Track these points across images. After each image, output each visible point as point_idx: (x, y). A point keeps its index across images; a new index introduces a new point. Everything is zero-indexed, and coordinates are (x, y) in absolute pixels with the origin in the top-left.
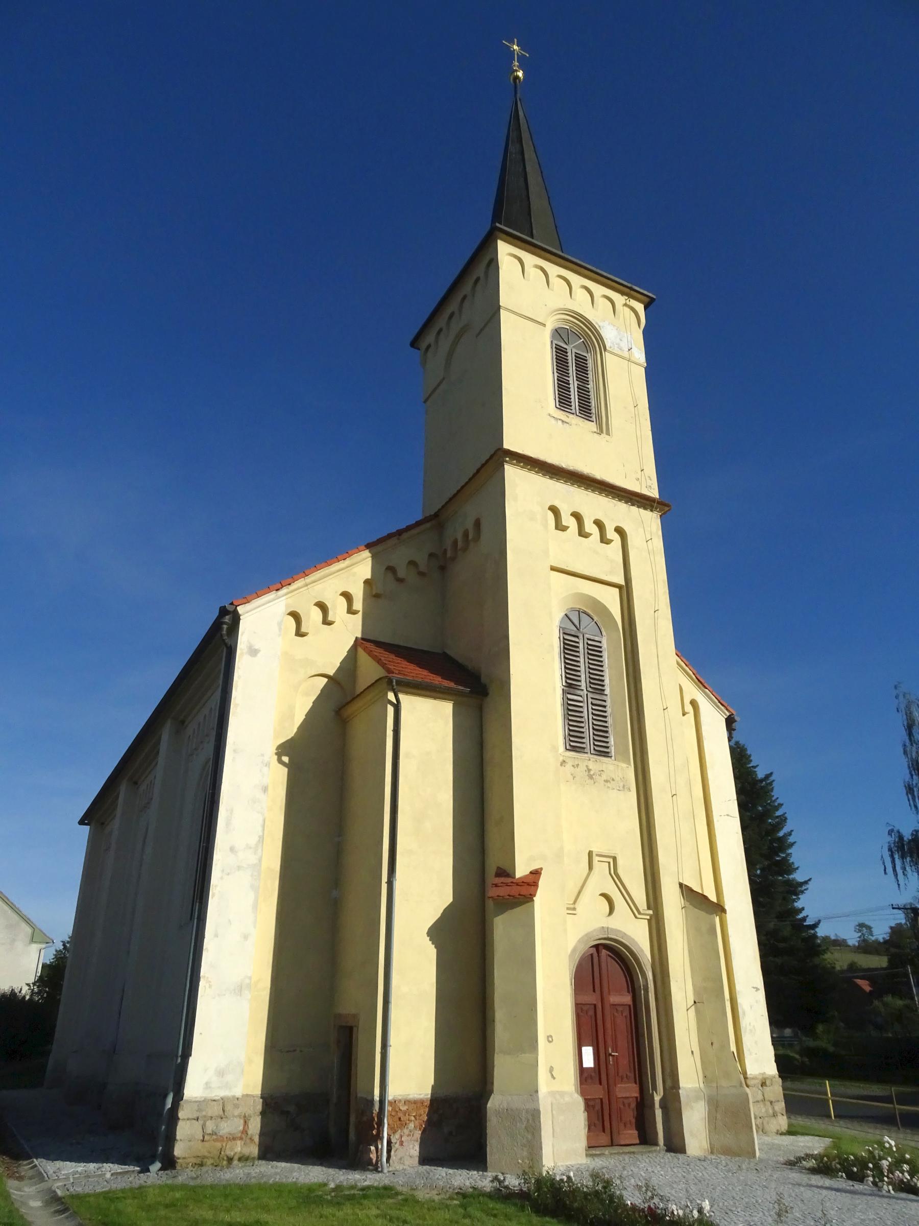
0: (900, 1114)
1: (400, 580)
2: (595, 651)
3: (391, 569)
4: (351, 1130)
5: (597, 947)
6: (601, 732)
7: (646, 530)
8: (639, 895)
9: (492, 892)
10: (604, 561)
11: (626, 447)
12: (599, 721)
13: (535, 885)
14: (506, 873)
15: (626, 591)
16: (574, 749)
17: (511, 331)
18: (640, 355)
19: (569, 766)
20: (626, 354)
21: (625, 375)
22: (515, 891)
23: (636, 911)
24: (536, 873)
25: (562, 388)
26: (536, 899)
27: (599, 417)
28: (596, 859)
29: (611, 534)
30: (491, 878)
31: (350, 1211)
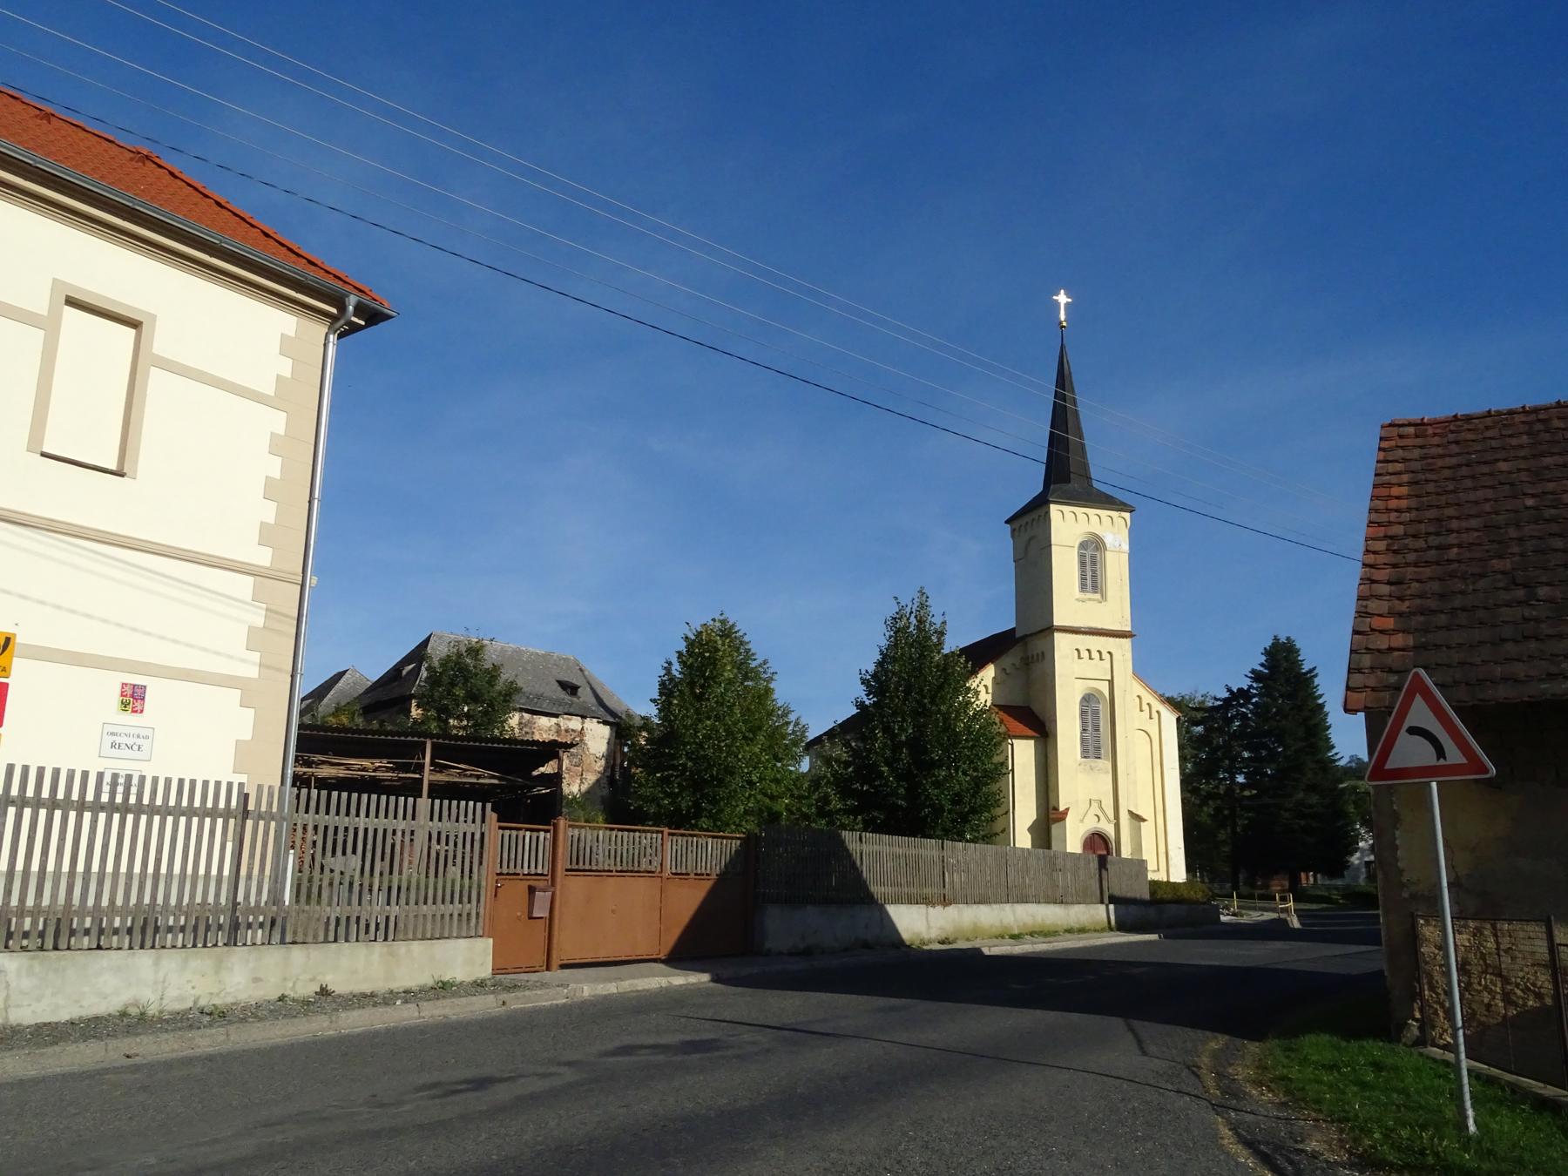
2: (1096, 713)
4: (1032, 909)
6: (1098, 748)
7: (1122, 650)
8: (1111, 815)
10: (1100, 669)
11: (1115, 609)
12: (1100, 739)
14: (1056, 809)
15: (1111, 682)
18: (1126, 547)
21: (1117, 567)
23: (1109, 821)
25: (1083, 578)
29: (1106, 656)
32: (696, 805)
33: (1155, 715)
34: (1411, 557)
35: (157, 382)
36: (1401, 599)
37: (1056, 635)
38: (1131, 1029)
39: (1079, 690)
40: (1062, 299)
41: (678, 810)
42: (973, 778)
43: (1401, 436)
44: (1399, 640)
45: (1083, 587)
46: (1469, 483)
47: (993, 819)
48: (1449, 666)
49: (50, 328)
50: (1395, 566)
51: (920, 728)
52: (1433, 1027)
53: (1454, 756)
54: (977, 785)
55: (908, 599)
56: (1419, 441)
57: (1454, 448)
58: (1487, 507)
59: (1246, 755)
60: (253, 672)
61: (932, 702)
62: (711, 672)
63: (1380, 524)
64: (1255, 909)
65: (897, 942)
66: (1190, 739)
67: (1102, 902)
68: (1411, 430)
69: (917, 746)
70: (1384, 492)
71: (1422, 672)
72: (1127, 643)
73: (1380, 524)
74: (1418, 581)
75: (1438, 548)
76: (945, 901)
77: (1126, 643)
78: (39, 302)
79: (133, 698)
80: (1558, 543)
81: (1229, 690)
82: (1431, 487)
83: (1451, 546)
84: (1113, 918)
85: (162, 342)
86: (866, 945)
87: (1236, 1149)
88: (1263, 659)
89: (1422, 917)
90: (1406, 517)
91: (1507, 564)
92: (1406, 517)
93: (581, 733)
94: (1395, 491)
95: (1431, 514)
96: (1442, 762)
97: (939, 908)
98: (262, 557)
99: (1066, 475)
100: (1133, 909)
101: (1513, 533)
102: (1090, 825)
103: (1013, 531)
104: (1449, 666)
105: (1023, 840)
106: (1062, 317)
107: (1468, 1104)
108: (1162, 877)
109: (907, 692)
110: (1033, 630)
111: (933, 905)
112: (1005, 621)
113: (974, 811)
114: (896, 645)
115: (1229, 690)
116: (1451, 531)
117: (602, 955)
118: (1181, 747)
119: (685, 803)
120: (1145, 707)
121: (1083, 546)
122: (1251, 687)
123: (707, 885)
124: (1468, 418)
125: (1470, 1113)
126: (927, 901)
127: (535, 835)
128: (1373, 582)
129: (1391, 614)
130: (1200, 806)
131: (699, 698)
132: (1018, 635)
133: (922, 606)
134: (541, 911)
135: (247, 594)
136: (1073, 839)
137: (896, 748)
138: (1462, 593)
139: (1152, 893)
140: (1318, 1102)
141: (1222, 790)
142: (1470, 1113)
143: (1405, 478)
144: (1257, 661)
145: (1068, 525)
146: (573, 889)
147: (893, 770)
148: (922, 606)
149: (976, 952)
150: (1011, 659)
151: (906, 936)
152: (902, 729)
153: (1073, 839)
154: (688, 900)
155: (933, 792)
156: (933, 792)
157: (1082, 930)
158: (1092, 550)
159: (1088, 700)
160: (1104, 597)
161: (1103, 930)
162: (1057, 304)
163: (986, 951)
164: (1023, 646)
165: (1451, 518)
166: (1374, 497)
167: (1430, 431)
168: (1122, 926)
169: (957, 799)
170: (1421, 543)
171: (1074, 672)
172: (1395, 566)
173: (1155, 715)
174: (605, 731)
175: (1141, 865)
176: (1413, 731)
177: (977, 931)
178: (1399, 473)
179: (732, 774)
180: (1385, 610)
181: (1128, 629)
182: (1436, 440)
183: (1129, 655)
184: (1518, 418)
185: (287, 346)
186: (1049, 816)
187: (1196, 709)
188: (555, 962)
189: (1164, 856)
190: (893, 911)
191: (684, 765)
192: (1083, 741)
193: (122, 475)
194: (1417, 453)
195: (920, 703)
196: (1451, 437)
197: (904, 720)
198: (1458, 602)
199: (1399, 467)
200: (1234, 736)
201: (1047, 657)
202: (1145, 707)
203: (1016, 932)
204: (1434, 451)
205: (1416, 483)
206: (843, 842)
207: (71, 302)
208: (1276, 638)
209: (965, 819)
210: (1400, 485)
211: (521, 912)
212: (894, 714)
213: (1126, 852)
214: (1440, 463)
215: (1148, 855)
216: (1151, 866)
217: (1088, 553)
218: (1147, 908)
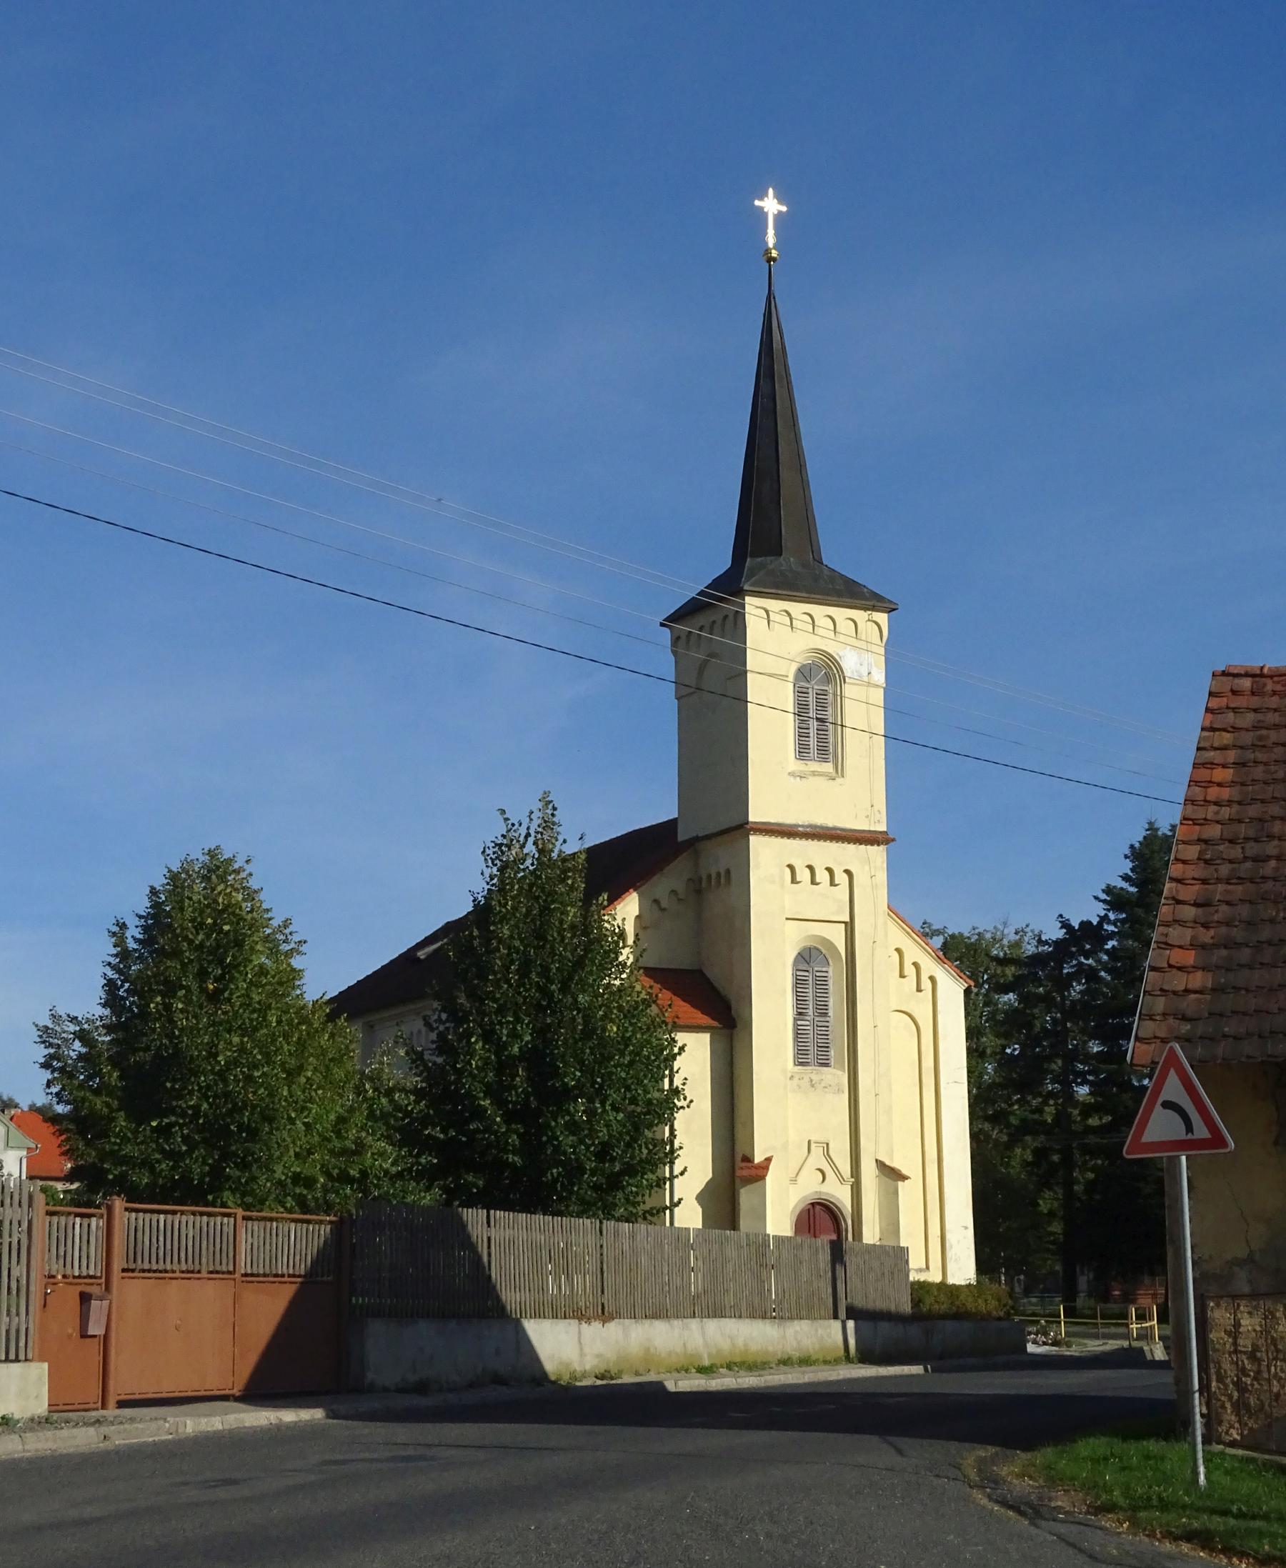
1: (663, 910)
2: (821, 982)
3: (656, 901)
5: (813, 1204)
7: (871, 865)
8: (846, 1169)
9: (739, 1173)
11: (858, 789)
12: (827, 1036)
13: (767, 1168)
14: (748, 1159)
15: (850, 927)
16: (801, 1064)
17: (756, 688)
18: (879, 677)
19: (796, 1080)
20: (866, 679)
22: (753, 1172)
23: (842, 1180)
24: (769, 1160)
25: (802, 734)
26: (768, 1178)
27: (836, 756)
28: (813, 1146)
29: (841, 878)
30: (739, 1163)
31: (798, 1328)
33: (927, 984)
34: (1225, 870)
36: (1206, 926)
37: (754, 840)
38: (890, 1444)
39: (791, 941)
40: (771, 205)
41: (186, 1178)
42: (630, 1115)
43: (1234, 692)
45: (802, 751)
47: (660, 1183)
48: (1244, 1014)
50: (1204, 882)
51: (542, 1033)
52: (1220, 1423)
53: (1201, 1132)
54: (637, 1128)
55: (524, 809)
56: (1255, 702)
59: (1095, 1048)
61: (564, 989)
63: (1195, 822)
64: (1096, 1337)
66: (992, 1017)
67: (836, 1317)
68: (1246, 683)
69: (539, 1061)
71: (1177, 1047)
73: (1195, 822)
74: (1228, 903)
75: (1255, 859)
76: (604, 1315)
77: (877, 854)
81: (1065, 925)
82: (1259, 772)
83: (1269, 858)
84: (852, 1342)
86: (498, 1380)
87: (990, 1505)
88: (1127, 867)
89: (1211, 1298)
90: (1226, 812)
92: (1226, 812)
95: (1253, 811)
96: (1190, 1136)
97: (596, 1325)
99: (772, 540)
100: (884, 1326)
102: (809, 1187)
103: (676, 641)
104: (1244, 1014)
105: (689, 1216)
106: (771, 240)
107: (1200, 1461)
108: (935, 1277)
110: (713, 828)
111: (589, 1320)
112: (655, 804)
113: (630, 1170)
114: (502, 890)
115: (1065, 925)
116: (1271, 837)
117: (167, 1388)
118: (972, 1033)
120: (910, 970)
121: (804, 673)
122: (1104, 919)
125: (1202, 1469)
126: (580, 1315)
127: (86, 1221)
128: (1178, 902)
129: (1193, 945)
130: (1009, 1146)
132: (682, 836)
133: (548, 824)
134: (95, 1329)
136: (778, 1211)
137: (504, 1066)
138: (1272, 921)
139: (916, 1303)
140: (1073, 1479)
142: (1202, 1469)
145: (778, 635)
147: (499, 1102)
150: (668, 882)
151: (550, 1366)
152: (514, 1035)
153: (778, 1211)
154: (267, 1310)
155: (567, 1140)
156: (567, 1140)
157: (805, 1361)
158: (818, 682)
159: (809, 958)
160: (839, 770)
161: (836, 1361)
162: (762, 214)
163: (671, 1386)
165: (1274, 818)
166: (1193, 782)
167: (1270, 686)
168: (866, 1355)
170: (1236, 852)
171: (782, 908)
172: (1204, 882)
173: (927, 984)
175: (900, 1255)
176: (1168, 1105)
177: (649, 1358)
178: (1224, 748)
179: (270, 1120)
180: (1187, 940)
181: (882, 827)
183: (882, 877)
186: (737, 1171)
187: (1003, 962)
188: (112, 1401)
189: (939, 1240)
191: (196, 1108)
192: (798, 1033)
194: (1250, 718)
195: (544, 991)
197: (518, 1020)
198: (1265, 934)
199: (1227, 738)
200: (1074, 1011)
201: (736, 878)
202: (910, 970)
203: (706, 1363)
205: (1244, 765)
206: (463, 1226)
208: (1152, 827)
209: (614, 1183)
210: (1224, 766)
211: (73, 1329)
212: (501, 1011)
213: (871, 1234)
215: (910, 1238)
216: (916, 1261)
217: (814, 686)
218: (913, 1324)
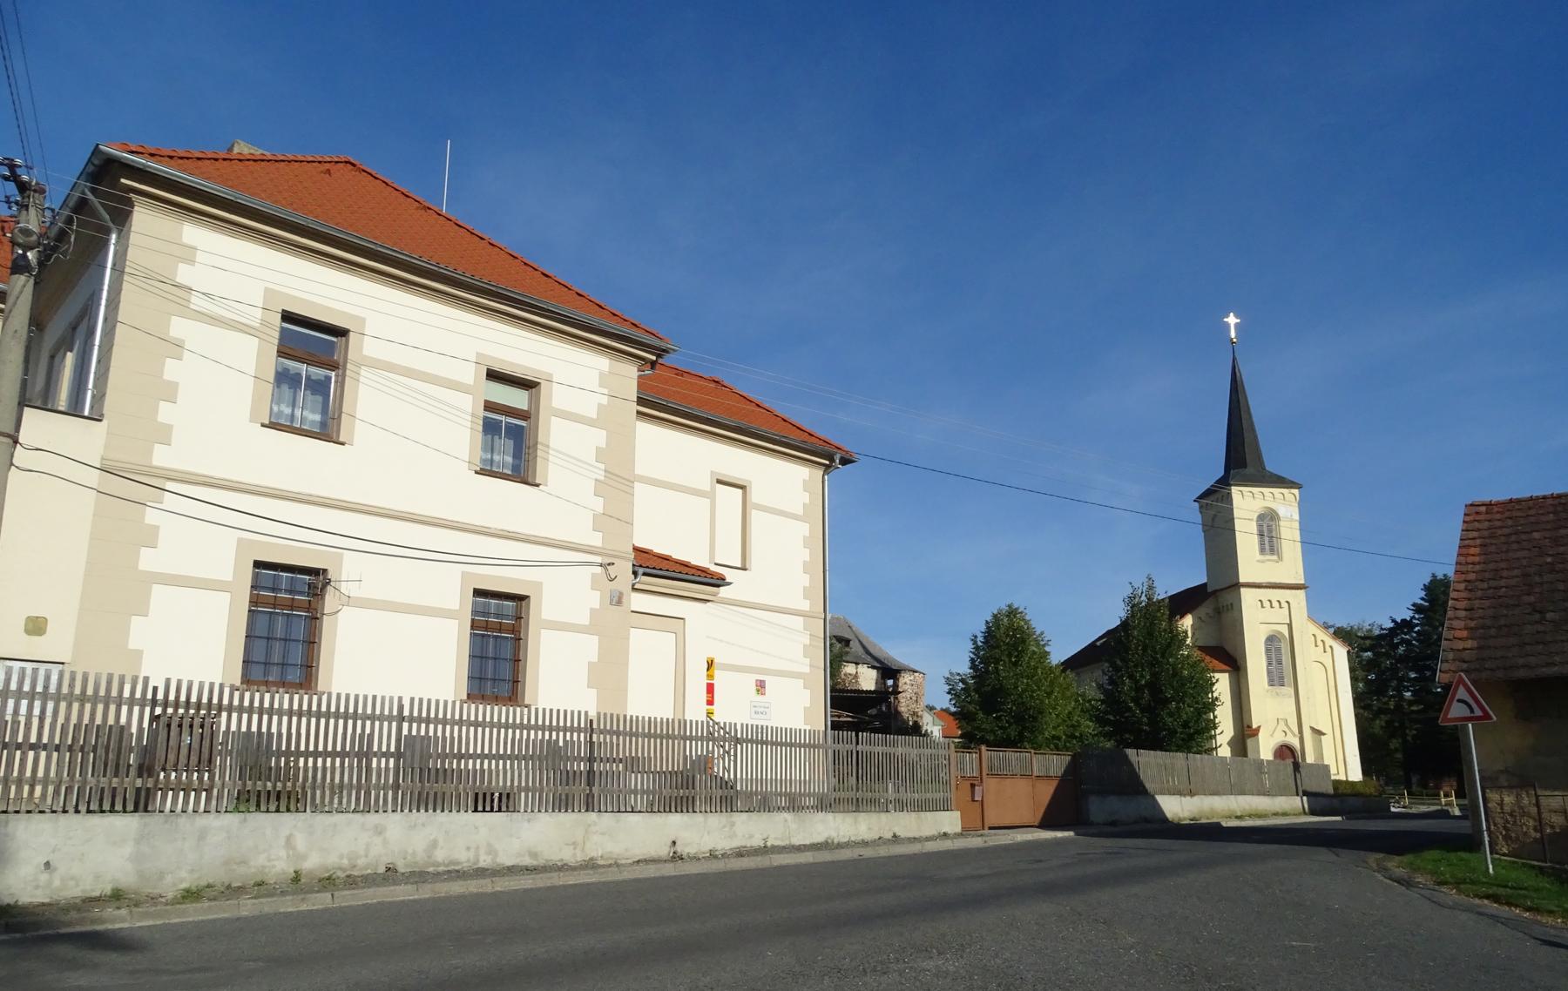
0: (308, 378)
2: (1278, 650)
4: (1249, 798)
6: (1282, 678)
7: (1298, 599)
8: (1296, 730)
11: (1291, 566)
12: (1283, 671)
14: (1250, 727)
15: (1290, 626)
18: (1296, 517)
25: (1262, 544)
32: (1021, 734)
34: (1479, 593)
35: (755, 515)
37: (1243, 590)
40: (1232, 320)
44: (1469, 644)
45: (1262, 551)
46: (1515, 546)
49: (711, 496)
51: (1154, 675)
53: (1478, 713)
56: (1489, 517)
57: (1510, 522)
58: (1524, 562)
59: (1413, 675)
60: (807, 670)
62: (1005, 643)
65: (1165, 820)
68: (1483, 509)
69: (1154, 687)
70: (1464, 551)
72: (1301, 593)
76: (1192, 794)
78: (705, 484)
79: (761, 686)
80: (1561, 586)
81: (1394, 621)
85: (755, 496)
86: (1146, 820)
88: (1423, 594)
90: (1478, 567)
91: (1532, 599)
92: (1478, 567)
93: (856, 676)
94: (1472, 550)
98: (805, 606)
99: (1242, 460)
101: (1537, 579)
102: (1279, 739)
105: (1225, 752)
106: (1233, 335)
109: (1144, 650)
112: (1195, 575)
115: (1394, 621)
118: (1352, 670)
119: (1013, 732)
121: (1261, 518)
123: (1055, 783)
124: (1519, 501)
126: (1181, 794)
129: (1466, 628)
131: (1015, 664)
133: (1151, 588)
135: (801, 627)
136: (1265, 748)
139: (1335, 789)
141: (1392, 705)
143: (1478, 542)
144: (1418, 596)
145: (1247, 502)
146: (991, 784)
148: (1151, 588)
149: (1218, 824)
150: (1204, 610)
153: (1265, 748)
154: (1047, 791)
159: (1272, 640)
160: (1280, 558)
162: (1228, 325)
163: (1224, 824)
164: (1215, 597)
168: (1313, 812)
169: (1185, 725)
170: (1485, 585)
171: (1257, 619)
174: (873, 674)
177: (1213, 812)
182: (1498, 516)
184: (1550, 501)
185: (806, 486)
186: (1245, 733)
189: (1343, 760)
190: (1159, 798)
192: (1269, 672)
193: (744, 569)
196: (1507, 514)
198: (1502, 622)
199: (1475, 534)
200: (1401, 659)
204: (1498, 524)
207: (719, 482)
208: (1434, 576)
209: (1191, 737)
214: (1499, 532)
215: (1329, 759)
216: (1333, 770)
218: (1337, 798)
